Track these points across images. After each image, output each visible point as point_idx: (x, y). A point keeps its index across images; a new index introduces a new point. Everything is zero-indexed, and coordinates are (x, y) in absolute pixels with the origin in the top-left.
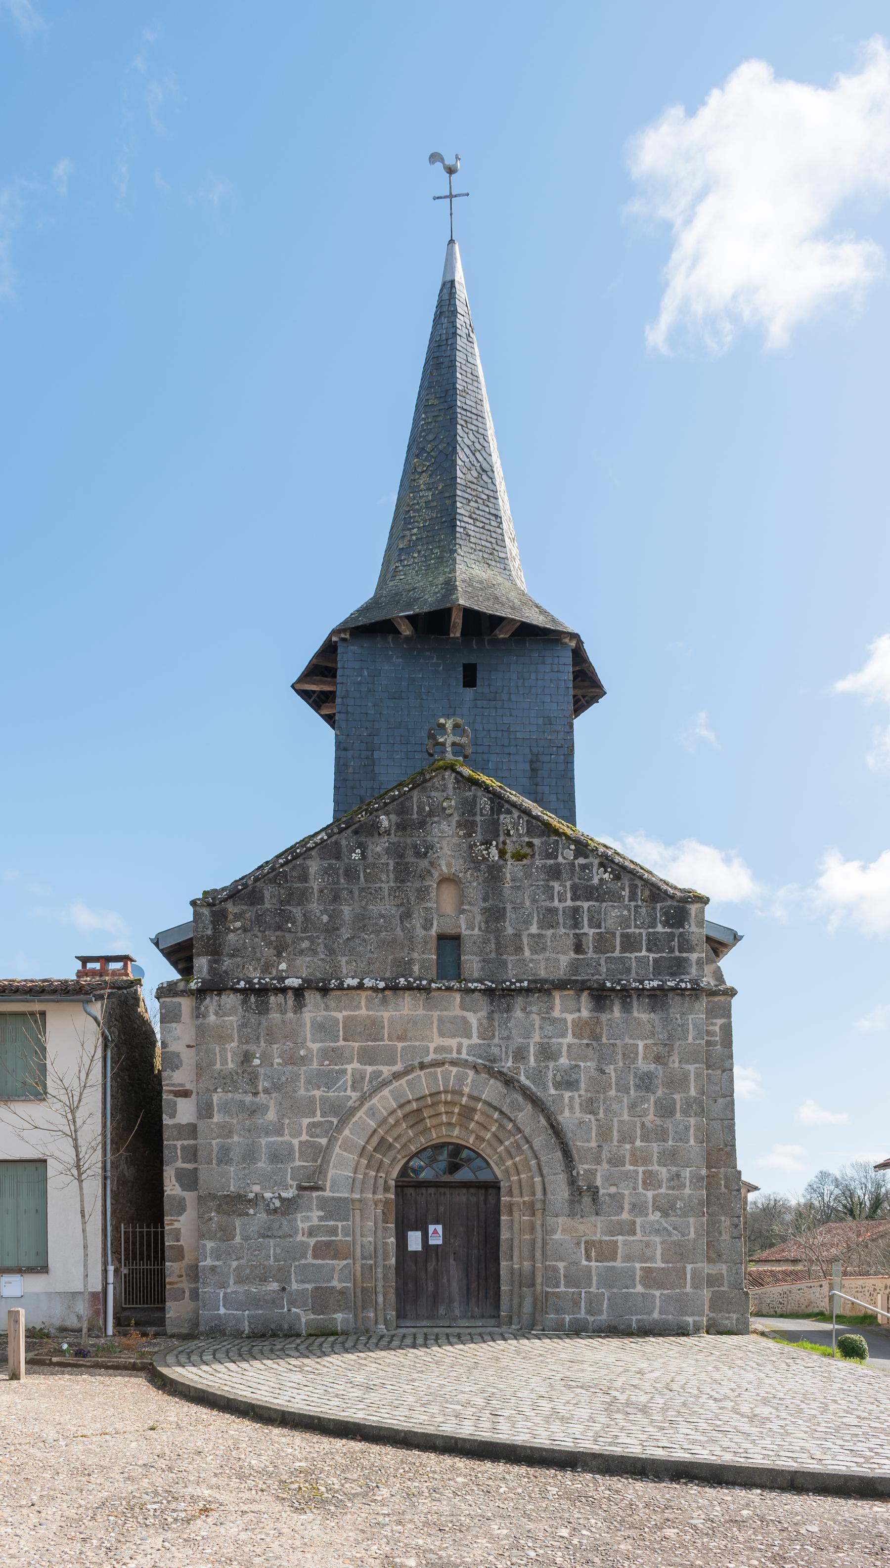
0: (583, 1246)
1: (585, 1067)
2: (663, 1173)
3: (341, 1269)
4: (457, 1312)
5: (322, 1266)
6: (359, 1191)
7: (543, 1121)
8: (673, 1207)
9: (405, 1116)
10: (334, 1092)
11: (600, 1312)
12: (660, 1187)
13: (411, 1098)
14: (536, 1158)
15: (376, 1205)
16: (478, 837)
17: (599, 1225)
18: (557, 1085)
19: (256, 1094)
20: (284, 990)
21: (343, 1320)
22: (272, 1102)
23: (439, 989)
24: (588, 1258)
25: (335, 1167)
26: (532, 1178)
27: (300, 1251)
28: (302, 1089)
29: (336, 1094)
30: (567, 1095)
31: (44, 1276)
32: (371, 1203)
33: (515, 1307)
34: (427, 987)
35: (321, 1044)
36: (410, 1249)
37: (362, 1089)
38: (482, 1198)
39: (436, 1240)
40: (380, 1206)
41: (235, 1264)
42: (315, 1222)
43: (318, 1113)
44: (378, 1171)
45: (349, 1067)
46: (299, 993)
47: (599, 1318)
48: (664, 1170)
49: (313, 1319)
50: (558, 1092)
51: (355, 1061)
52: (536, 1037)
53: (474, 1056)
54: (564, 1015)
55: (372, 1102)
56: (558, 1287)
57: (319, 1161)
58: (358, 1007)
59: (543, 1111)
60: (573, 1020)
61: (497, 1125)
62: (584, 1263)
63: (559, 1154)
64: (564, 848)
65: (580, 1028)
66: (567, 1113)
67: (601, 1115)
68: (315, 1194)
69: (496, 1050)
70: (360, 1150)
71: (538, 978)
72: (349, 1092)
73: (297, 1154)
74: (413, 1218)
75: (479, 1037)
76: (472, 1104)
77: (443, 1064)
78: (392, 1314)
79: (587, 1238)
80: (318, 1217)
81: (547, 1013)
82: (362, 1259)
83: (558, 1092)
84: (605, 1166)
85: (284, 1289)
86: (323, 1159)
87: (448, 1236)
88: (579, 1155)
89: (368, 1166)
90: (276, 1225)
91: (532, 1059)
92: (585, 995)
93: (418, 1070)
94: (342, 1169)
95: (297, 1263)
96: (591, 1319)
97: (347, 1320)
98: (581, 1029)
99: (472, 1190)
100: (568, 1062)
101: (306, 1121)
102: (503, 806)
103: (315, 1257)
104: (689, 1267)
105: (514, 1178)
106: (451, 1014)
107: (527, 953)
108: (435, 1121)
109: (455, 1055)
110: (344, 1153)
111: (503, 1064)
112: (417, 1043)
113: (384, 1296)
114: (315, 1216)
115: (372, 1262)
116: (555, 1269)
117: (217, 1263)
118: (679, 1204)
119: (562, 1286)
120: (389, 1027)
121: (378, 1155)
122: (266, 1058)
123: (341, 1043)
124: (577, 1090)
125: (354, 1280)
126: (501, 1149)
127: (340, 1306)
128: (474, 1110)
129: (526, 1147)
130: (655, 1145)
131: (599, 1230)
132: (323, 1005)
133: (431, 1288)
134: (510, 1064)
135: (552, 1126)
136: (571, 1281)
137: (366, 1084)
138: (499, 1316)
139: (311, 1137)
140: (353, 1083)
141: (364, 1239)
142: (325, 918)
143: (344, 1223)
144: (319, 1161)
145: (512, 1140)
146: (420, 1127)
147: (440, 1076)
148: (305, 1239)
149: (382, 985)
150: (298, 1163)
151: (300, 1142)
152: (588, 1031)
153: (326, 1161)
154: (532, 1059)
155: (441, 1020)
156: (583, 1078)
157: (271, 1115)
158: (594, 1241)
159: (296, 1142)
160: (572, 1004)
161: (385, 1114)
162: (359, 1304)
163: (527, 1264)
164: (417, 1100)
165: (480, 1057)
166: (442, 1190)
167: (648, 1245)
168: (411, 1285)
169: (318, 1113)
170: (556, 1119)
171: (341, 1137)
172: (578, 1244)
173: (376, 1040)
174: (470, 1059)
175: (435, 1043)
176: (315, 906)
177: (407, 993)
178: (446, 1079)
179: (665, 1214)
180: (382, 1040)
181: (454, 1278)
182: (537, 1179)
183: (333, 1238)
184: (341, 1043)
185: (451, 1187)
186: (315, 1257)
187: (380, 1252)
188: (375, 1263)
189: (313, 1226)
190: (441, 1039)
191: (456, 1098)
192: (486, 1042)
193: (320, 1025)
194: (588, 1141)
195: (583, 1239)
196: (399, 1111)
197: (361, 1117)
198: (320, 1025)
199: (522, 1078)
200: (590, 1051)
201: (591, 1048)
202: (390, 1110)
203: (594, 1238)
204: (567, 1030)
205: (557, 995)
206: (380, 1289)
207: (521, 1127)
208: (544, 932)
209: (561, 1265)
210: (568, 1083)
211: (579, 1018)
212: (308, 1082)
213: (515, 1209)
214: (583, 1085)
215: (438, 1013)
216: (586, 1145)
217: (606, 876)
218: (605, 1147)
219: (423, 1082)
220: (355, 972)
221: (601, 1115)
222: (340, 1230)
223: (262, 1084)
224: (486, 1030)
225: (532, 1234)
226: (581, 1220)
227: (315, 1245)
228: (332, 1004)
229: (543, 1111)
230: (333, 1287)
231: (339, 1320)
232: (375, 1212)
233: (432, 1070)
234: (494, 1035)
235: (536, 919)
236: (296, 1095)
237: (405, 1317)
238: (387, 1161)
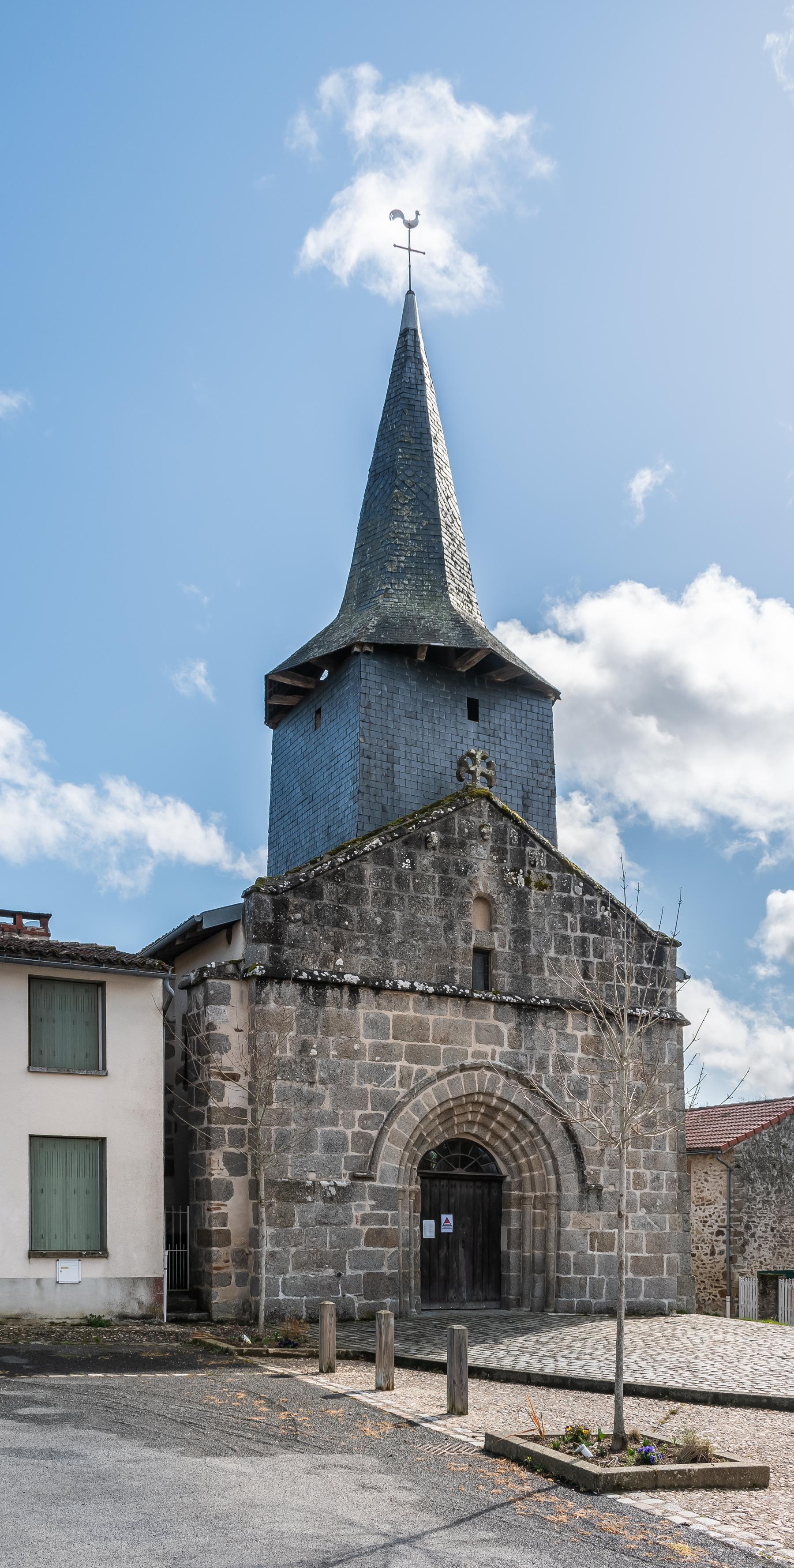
0: (588, 1237)
2: (648, 1175)
3: (391, 1256)
4: (465, 1296)
5: (374, 1252)
8: (654, 1205)
10: (384, 1086)
11: (600, 1296)
12: (645, 1187)
16: (508, 864)
19: (312, 1084)
20: (340, 986)
22: (327, 1092)
23: (480, 999)
24: (592, 1249)
25: (384, 1158)
27: (351, 1239)
28: (356, 1082)
31: (104, 1261)
37: (409, 1086)
38: (486, 1191)
39: (447, 1229)
41: (293, 1250)
42: (368, 1210)
45: (398, 1064)
46: (354, 989)
48: (648, 1172)
49: (365, 1304)
54: (576, 1032)
55: (417, 1098)
56: (569, 1274)
58: (407, 1008)
60: (582, 1037)
62: (590, 1252)
64: (575, 885)
68: (367, 1184)
69: (522, 1059)
72: (397, 1088)
75: (509, 1046)
76: (500, 1105)
77: (481, 1067)
79: (592, 1230)
80: (370, 1205)
81: (562, 1029)
83: (571, 1100)
84: (606, 1167)
85: (339, 1275)
90: (333, 1212)
96: (593, 1301)
99: (478, 1184)
101: (358, 1113)
102: (528, 839)
103: (367, 1244)
104: (666, 1256)
107: (547, 974)
108: (462, 1119)
112: (458, 1047)
116: (567, 1258)
117: (277, 1249)
118: (659, 1202)
120: (434, 1030)
122: (322, 1048)
123: (391, 1041)
130: (642, 1150)
133: (443, 1273)
134: (533, 1072)
136: (579, 1269)
142: (379, 920)
148: (358, 1227)
149: (431, 990)
151: (353, 1133)
155: (478, 1028)
157: (327, 1105)
159: (349, 1133)
161: (428, 1110)
163: (538, 1253)
165: (510, 1064)
166: (453, 1182)
167: (636, 1237)
172: (585, 1235)
173: (422, 1040)
175: (473, 1048)
176: (369, 908)
178: (482, 1082)
179: (649, 1211)
180: (427, 1041)
183: (384, 1226)
184: (391, 1041)
186: (367, 1244)
189: (366, 1214)
190: (478, 1045)
192: (514, 1050)
193: (372, 1023)
195: (589, 1231)
197: (407, 1112)
203: (597, 1231)
208: (559, 957)
209: (571, 1254)
210: (580, 1094)
212: (361, 1076)
214: (590, 1095)
215: (476, 1020)
216: (592, 1148)
217: (606, 913)
218: (607, 1151)
219: (462, 1084)
223: (319, 1074)
226: (588, 1214)
227: (367, 1233)
233: (470, 1072)
234: (521, 1045)
235: (553, 944)
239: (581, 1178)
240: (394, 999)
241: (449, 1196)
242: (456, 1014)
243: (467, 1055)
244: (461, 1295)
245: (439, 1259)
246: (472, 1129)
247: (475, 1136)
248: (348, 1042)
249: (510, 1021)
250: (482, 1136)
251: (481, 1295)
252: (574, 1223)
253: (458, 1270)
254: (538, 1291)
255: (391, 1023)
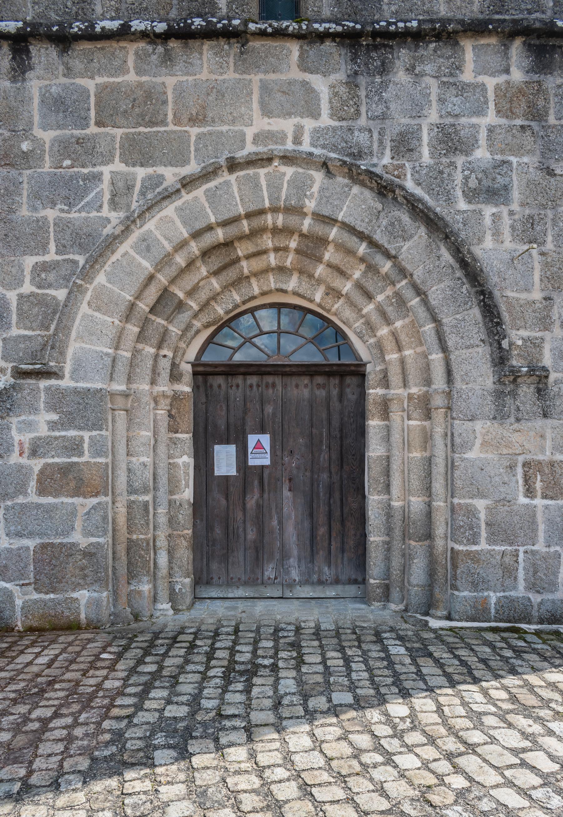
0: (520, 471)
1: (519, 164)
3: (88, 513)
4: (295, 574)
5: (54, 507)
6: (124, 378)
7: (447, 256)
9: (206, 254)
10: (79, 211)
13: (213, 220)
14: (435, 319)
15: (156, 402)
17: (549, 435)
18: (471, 195)
21: (89, 604)
23: (262, 34)
24: (530, 492)
25: (80, 337)
26: (425, 356)
28: (25, 207)
29: (83, 214)
30: (489, 211)
32: (146, 399)
33: (395, 572)
34: (242, 28)
35: (58, 132)
36: (217, 473)
37: (129, 206)
38: (335, 392)
39: (260, 459)
40: (164, 404)
42: (43, 431)
43: (52, 247)
44: (159, 347)
45: (106, 170)
47: (550, 596)
49: (36, 602)
50: (472, 207)
51: (117, 159)
52: (433, 116)
53: (324, 147)
54: (481, 79)
55: (146, 227)
56: (475, 543)
57: (53, 327)
58: (122, 70)
59: (447, 237)
60: (497, 88)
61: (363, 267)
62: (523, 500)
63: (476, 313)
65: (507, 100)
66: (489, 242)
67: (550, 246)
68: (43, 384)
69: (362, 138)
70: (123, 307)
71: (435, 17)
72: (106, 212)
73: (14, 317)
74: (222, 424)
75: (332, 116)
76: (320, 230)
77: (270, 160)
78: (184, 582)
79: (529, 457)
80: (48, 423)
81: (451, 75)
82: (130, 493)
86: (58, 325)
87: (279, 453)
88: (511, 315)
89: (141, 337)
91: (426, 151)
92: (517, 47)
93: (226, 173)
94: (91, 343)
95: (9, 503)
96: (536, 598)
97: (97, 603)
98: (511, 101)
99: (320, 380)
100: (488, 155)
101: (30, 261)
103: (42, 491)
105: (392, 357)
106: (283, 77)
108: (257, 264)
109: (289, 146)
110: (96, 314)
111: (375, 160)
112: (225, 128)
113: (171, 552)
114: (43, 421)
115: (148, 498)
116: (471, 512)
119: (483, 540)
120: (175, 102)
121: (159, 320)
123: (93, 129)
124: (507, 202)
125: (114, 530)
126: (369, 308)
127: (85, 577)
128: (323, 241)
129: (415, 302)
131: (549, 444)
132: (61, 68)
133: (251, 535)
134: (386, 160)
135: (464, 264)
136: (497, 532)
137: (135, 197)
138: (364, 581)
139: (39, 287)
140: (114, 195)
141: (134, 459)
143: (94, 433)
144: (53, 327)
145: (389, 291)
146: (231, 274)
147: (263, 183)
148: (24, 461)
150: (15, 332)
151: (21, 297)
152: (524, 105)
153: (64, 328)
154: (426, 151)
155: (265, 88)
156: (515, 183)
158: (540, 463)
160: (495, 61)
161: (169, 247)
162: (123, 571)
163: (417, 502)
164: (224, 224)
165: (334, 148)
166: (270, 379)
168: (218, 531)
169: (52, 247)
170: (469, 252)
171: (91, 287)
172: (511, 467)
173: (155, 124)
174: (317, 151)
175: (254, 127)
177: (207, 45)
178: (274, 188)
180: (163, 123)
181: (289, 517)
182: (437, 357)
183: (75, 459)
184: (93, 129)
185: (284, 374)
186: (42, 491)
187: (163, 481)
188: (155, 498)
189: (39, 438)
190: (266, 120)
191: (293, 220)
192: (344, 123)
193: (56, 100)
194: (527, 290)
196: (193, 244)
197: (126, 253)
198: (56, 100)
199: (409, 184)
200: (527, 139)
201: (528, 133)
202: (176, 241)
203: (540, 457)
204: (486, 102)
205: (468, 46)
206: (162, 542)
207: (409, 267)
209: (481, 504)
210: (491, 191)
211: (508, 82)
212: (36, 195)
213: (394, 406)
214: (516, 194)
215: (261, 76)
216: (523, 296)
219: (235, 193)
220: (117, 10)
221: (550, 246)
222: (86, 446)
224: (344, 103)
225: (425, 449)
226: (516, 426)
227: (42, 472)
228: (77, 64)
229: (447, 237)
230: (73, 544)
231: (83, 602)
232: (155, 415)
233: (251, 172)
234: (358, 113)
236: (14, 217)
237: (209, 583)
238: (175, 330)
239: (496, 355)
240: (98, 55)
241: (262, 402)
242: (221, 68)
243: (243, 141)
244: (288, 573)
245: (244, 509)
246: (287, 282)
247: (296, 294)
248: (9, 139)
249: (335, 71)
250: (308, 294)
251: (327, 573)
252: (485, 444)
253: (282, 529)
254: (418, 573)
255: (92, 100)
